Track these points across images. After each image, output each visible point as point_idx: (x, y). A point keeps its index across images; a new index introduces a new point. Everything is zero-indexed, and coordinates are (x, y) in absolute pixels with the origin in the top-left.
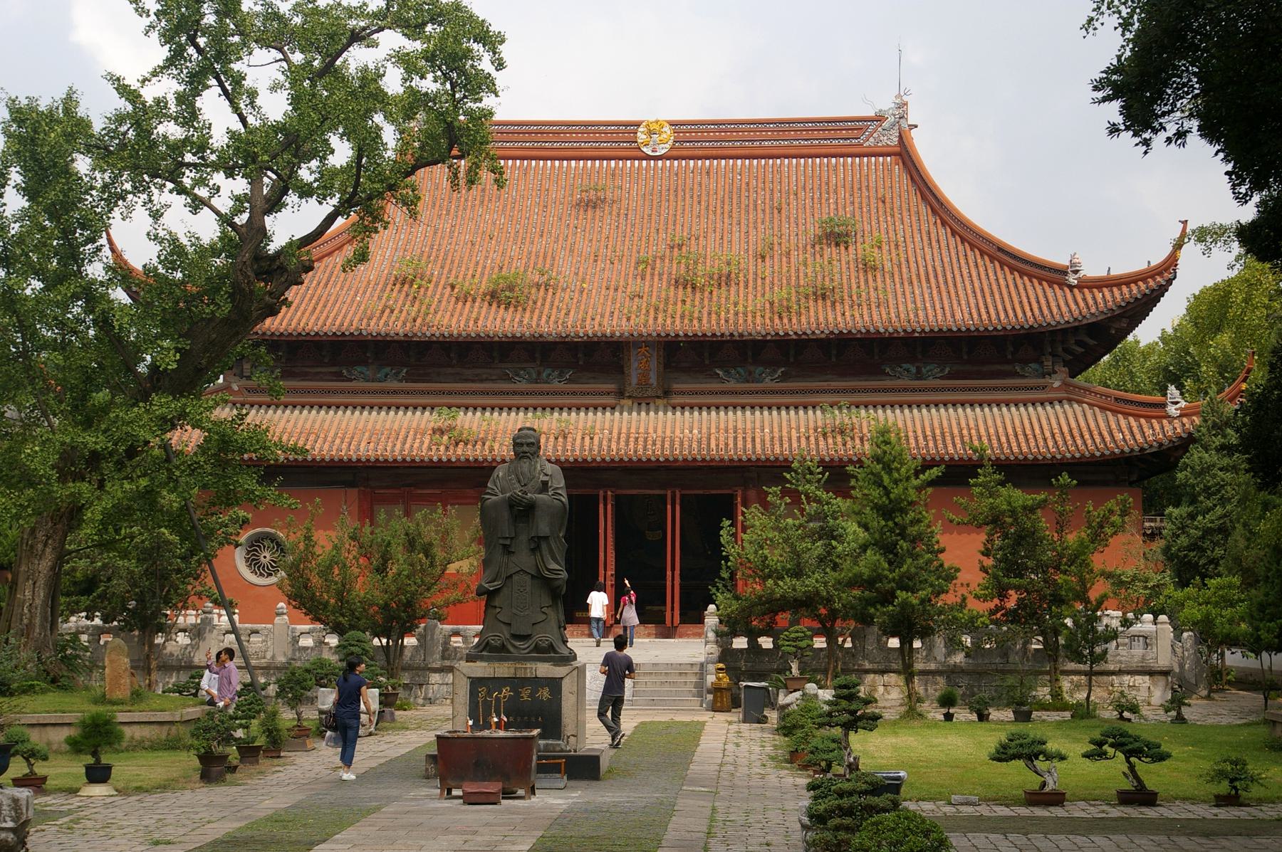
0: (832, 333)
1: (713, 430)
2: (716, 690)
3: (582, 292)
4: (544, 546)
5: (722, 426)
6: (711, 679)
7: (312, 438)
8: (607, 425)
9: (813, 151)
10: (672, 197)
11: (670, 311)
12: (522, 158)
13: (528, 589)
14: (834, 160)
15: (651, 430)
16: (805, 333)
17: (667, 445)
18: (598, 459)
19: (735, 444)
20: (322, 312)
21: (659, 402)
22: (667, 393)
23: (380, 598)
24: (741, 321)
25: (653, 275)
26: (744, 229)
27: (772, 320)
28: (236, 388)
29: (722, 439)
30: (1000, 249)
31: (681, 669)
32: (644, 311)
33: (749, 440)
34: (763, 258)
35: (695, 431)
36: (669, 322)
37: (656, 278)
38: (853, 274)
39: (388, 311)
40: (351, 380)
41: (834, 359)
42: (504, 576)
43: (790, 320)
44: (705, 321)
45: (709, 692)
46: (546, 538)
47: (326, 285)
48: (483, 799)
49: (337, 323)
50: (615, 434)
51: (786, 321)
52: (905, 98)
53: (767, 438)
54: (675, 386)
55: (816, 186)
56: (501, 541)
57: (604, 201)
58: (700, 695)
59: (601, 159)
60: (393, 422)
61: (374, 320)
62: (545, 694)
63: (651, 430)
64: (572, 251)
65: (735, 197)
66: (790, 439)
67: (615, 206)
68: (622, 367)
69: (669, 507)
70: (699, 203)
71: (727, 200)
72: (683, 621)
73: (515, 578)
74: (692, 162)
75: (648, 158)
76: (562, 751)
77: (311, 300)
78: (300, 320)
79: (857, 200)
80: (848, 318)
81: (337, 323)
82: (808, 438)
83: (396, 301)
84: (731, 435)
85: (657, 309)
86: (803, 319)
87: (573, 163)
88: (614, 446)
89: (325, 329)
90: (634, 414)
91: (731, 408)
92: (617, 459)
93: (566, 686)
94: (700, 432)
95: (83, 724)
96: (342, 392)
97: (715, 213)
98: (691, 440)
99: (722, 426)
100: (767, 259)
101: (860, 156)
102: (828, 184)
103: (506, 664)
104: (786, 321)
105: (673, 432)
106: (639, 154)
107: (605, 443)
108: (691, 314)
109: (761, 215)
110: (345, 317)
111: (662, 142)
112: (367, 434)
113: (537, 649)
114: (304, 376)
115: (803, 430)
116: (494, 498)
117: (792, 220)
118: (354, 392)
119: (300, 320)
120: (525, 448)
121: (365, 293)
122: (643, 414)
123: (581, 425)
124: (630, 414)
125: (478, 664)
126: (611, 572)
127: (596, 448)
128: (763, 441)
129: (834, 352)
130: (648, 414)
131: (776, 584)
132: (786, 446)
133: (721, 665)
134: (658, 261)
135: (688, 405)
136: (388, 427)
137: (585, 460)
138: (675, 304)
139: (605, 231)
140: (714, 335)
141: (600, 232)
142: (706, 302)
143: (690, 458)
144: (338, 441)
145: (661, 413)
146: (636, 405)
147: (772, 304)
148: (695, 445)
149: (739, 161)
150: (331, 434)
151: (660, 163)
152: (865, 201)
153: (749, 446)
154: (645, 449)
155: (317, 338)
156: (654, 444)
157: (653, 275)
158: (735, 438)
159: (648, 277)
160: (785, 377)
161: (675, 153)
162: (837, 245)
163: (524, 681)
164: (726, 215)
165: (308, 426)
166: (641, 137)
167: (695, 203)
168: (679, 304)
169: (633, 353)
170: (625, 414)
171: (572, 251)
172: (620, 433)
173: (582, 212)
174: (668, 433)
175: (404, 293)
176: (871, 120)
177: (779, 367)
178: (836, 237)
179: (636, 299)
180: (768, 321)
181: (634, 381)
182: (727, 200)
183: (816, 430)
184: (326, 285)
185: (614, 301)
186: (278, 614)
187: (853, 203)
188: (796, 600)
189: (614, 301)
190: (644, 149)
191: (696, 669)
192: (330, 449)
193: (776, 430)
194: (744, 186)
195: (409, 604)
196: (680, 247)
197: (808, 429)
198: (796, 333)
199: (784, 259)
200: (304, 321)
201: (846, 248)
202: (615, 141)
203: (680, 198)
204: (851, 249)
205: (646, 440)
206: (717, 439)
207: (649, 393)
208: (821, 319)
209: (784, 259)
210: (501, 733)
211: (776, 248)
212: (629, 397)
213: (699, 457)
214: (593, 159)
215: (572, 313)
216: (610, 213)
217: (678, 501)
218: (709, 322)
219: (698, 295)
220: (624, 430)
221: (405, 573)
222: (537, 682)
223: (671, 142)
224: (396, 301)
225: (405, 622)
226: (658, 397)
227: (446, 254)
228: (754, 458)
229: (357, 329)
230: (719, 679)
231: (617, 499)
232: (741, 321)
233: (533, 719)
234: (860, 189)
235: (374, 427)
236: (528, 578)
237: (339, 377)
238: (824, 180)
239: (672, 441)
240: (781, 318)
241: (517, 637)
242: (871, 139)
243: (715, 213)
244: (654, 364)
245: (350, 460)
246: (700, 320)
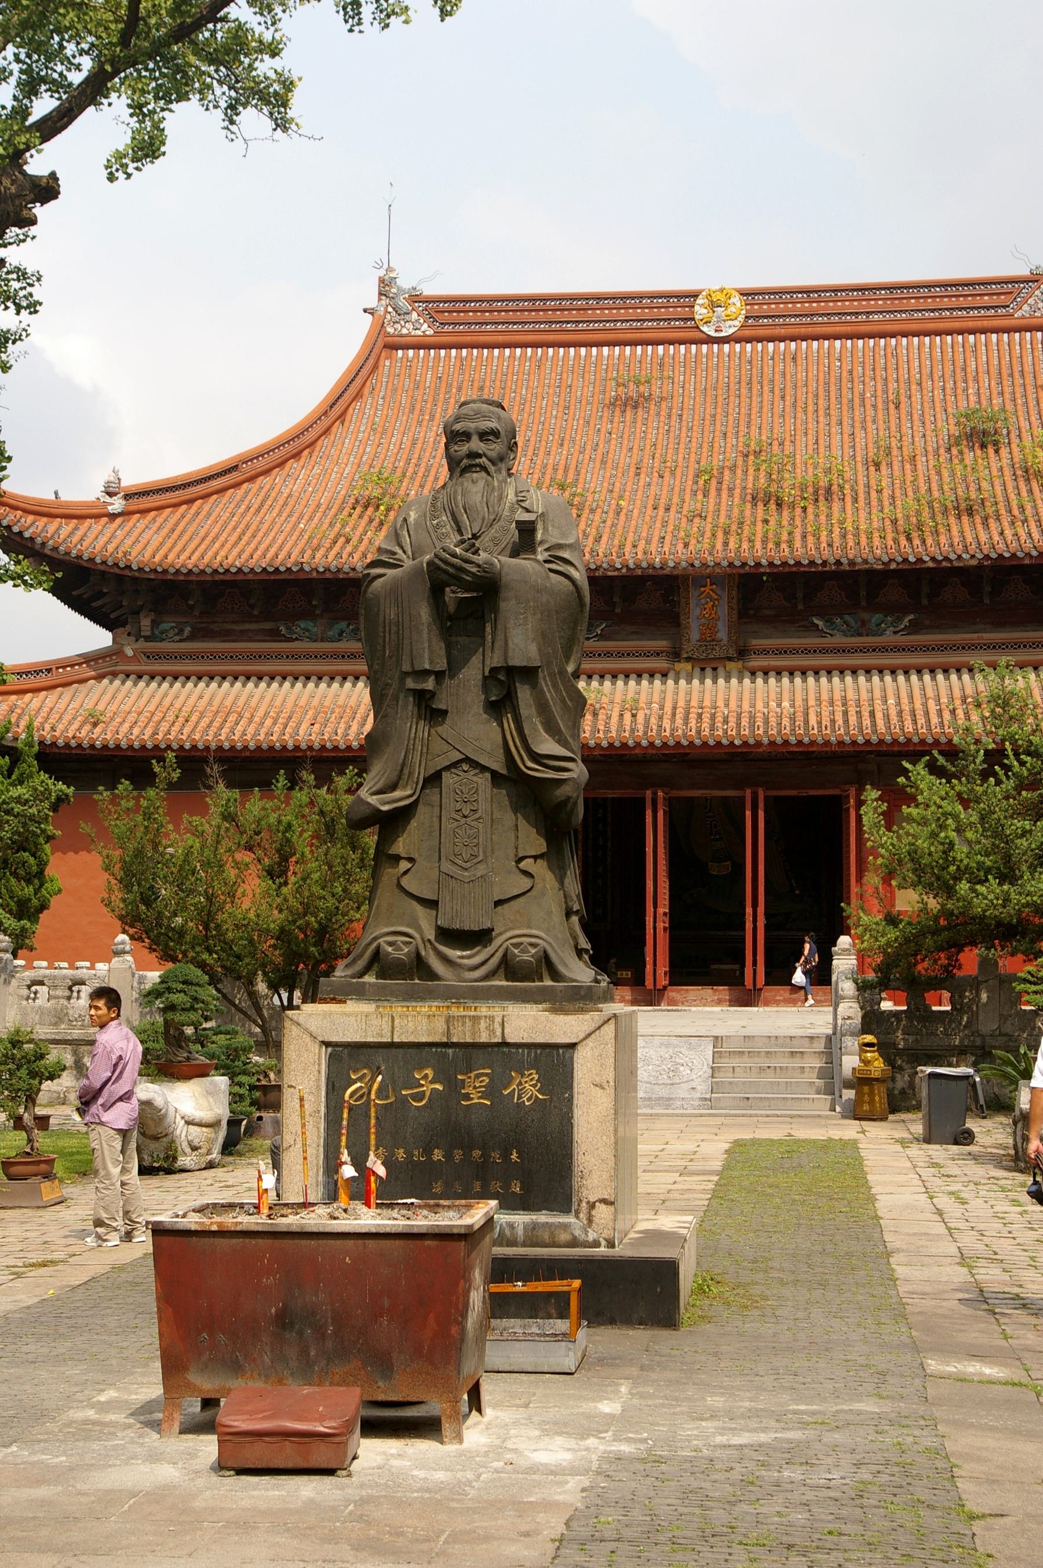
0: (987, 557)
1: (812, 702)
2: (861, 1082)
3: (618, 514)
4: (524, 694)
5: (825, 696)
6: (850, 1062)
7: (232, 718)
8: (656, 698)
9: (942, 326)
10: (744, 391)
11: (746, 533)
12: (535, 345)
13: (483, 807)
14: (971, 338)
15: (720, 703)
16: (946, 559)
17: (745, 722)
18: (644, 743)
19: (846, 721)
20: (248, 544)
21: (731, 665)
22: (742, 653)
23: (277, 919)
24: (851, 543)
25: (719, 490)
26: (847, 430)
27: (896, 541)
28: (129, 652)
29: (825, 714)
31: (792, 1047)
32: (708, 534)
33: (866, 714)
34: (877, 465)
35: (786, 704)
36: (745, 546)
37: (724, 494)
38: (1010, 485)
39: (342, 540)
40: (292, 640)
41: (987, 601)
42: (420, 773)
43: (924, 542)
44: (798, 543)
45: (848, 1085)
46: (529, 673)
47: (258, 510)
48: (288, 1454)
49: (269, 556)
50: (668, 709)
51: (917, 542)
53: (893, 712)
54: (754, 642)
55: (948, 372)
56: (410, 683)
57: (648, 399)
58: (829, 1090)
59: (645, 343)
60: (349, 697)
61: (322, 551)
62: (527, 1088)
63: (720, 703)
64: (603, 462)
65: (833, 388)
66: (927, 713)
67: (664, 404)
68: (677, 617)
69: (748, 813)
70: (783, 398)
71: (822, 393)
72: (767, 984)
73: (448, 778)
74: (771, 345)
75: (710, 340)
76: (574, 1243)
77: (235, 528)
78: (217, 554)
79: (1008, 390)
80: (1009, 538)
81: (269, 556)
82: (953, 712)
83: (354, 528)
84: (839, 709)
85: (726, 533)
86: (943, 539)
87: (605, 349)
88: (667, 724)
89: (252, 563)
90: (696, 682)
91: (836, 672)
92: (671, 743)
93: (590, 1068)
94: (793, 706)
96: (279, 656)
97: (805, 412)
98: (780, 717)
99: (825, 696)
100: (883, 467)
101: (1008, 330)
102: (964, 370)
103: (424, 1008)
104: (917, 542)
105: (753, 706)
106: (696, 335)
107: (653, 721)
108: (777, 534)
109: (870, 412)
110: (280, 548)
111: (729, 318)
112: (310, 713)
113: (509, 968)
114: (226, 635)
115: (944, 700)
116: (390, 572)
117: (916, 417)
118: (295, 656)
119: (217, 554)
120: (476, 444)
121: (311, 518)
122: (708, 682)
123: (618, 698)
124: (689, 682)
125: (352, 1006)
126: (663, 909)
127: (641, 727)
128: (887, 717)
129: (988, 589)
130: (715, 682)
131: (973, 890)
132: (921, 721)
133: (869, 1038)
134: (727, 472)
135: (773, 669)
136: (340, 702)
137: (624, 745)
138: (754, 523)
139: (651, 436)
140: (812, 563)
141: (644, 438)
142: (798, 522)
143: (779, 740)
144: (268, 722)
145: (734, 681)
146: (697, 670)
147: (894, 522)
148: (786, 722)
149: (838, 343)
150: (261, 713)
151: (726, 347)
152: (1019, 391)
153: (867, 722)
154: (712, 728)
155: (240, 577)
156: (726, 721)
157: (719, 490)
158: (845, 713)
159: (713, 493)
160: (914, 628)
161: (747, 333)
162: (983, 446)
163: (472, 1052)
164: (821, 412)
165: (228, 702)
166: (700, 311)
167: (777, 398)
168: (759, 524)
169: (693, 593)
170: (682, 682)
171: (603, 462)
172: (675, 708)
173: (618, 412)
174: (746, 707)
175: (366, 518)
176: (1026, 281)
177: (906, 613)
178: (981, 437)
179: (697, 520)
180: (890, 543)
181: (695, 635)
182: (822, 393)
183: (964, 701)
184: (258, 510)
185: (665, 524)
186: (118, 953)
187: (1002, 394)
188: (999, 924)
189: (665, 524)
190: (705, 329)
191: (820, 1046)
192: (257, 733)
193: (905, 700)
194: (845, 374)
195: (323, 932)
196: (757, 454)
197: (952, 699)
198: (933, 559)
199: (908, 466)
200: (223, 553)
201: (997, 451)
202: (663, 318)
203: (755, 392)
204: (1004, 452)
205: (713, 717)
206: (819, 714)
207: (717, 653)
208: (969, 538)
209: (908, 466)
210: (367, 1219)
211: (895, 452)
212: (688, 659)
213: (793, 740)
214: (634, 343)
215: (605, 539)
216: (658, 414)
217: (761, 805)
218: (805, 546)
219: (786, 513)
220: (681, 703)
221: (315, 876)
222: (504, 1053)
223: (741, 318)
224: (354, 528)
225: (318, 963)
226: (730, 659)
227: (428, 470)
228: (874, 739)
229: (296, 564)
230: (866, 1062)
231: (670, 802)
232: (851, 543)
233: (496, 1156)
234: (1012, 375)
235: (321, 704)
236: (483, 781)
237: (275, 635)
238: (960, 362)
239: (752, 718)
240: (909, 539)
241: (450, 936)
242: (1026, 307)
243: (805, 412)
244: (723, 610)
245: (284, 747)
246: (790, 543)
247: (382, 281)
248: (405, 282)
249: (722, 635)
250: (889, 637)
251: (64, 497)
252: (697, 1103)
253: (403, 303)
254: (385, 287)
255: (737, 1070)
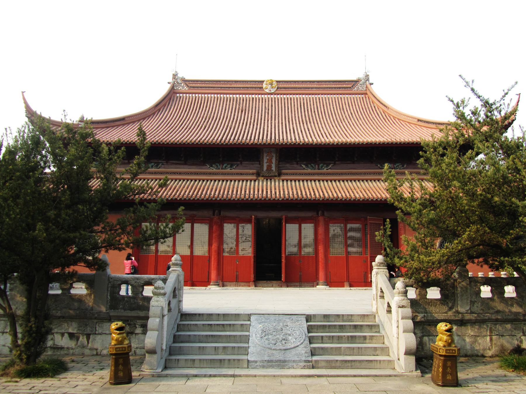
22: (280, 175)
30: (419, 120)
52: (368, 74)
54: (283, 171)
95: (77, 265)
161: (277, 92)
166: (264, 86)
181: (265, 168)
202: (255, 86)
207: (272, 174)
212: (263, 176)
226: (276, 176)
247: (173, 75)
248: (180, 75)
249: (274, 168)
250: (325, 170)
251: (52, 118)
252: (302, 364)
253: (179, 81)
254: (175, 76)
255: (324, 338)
